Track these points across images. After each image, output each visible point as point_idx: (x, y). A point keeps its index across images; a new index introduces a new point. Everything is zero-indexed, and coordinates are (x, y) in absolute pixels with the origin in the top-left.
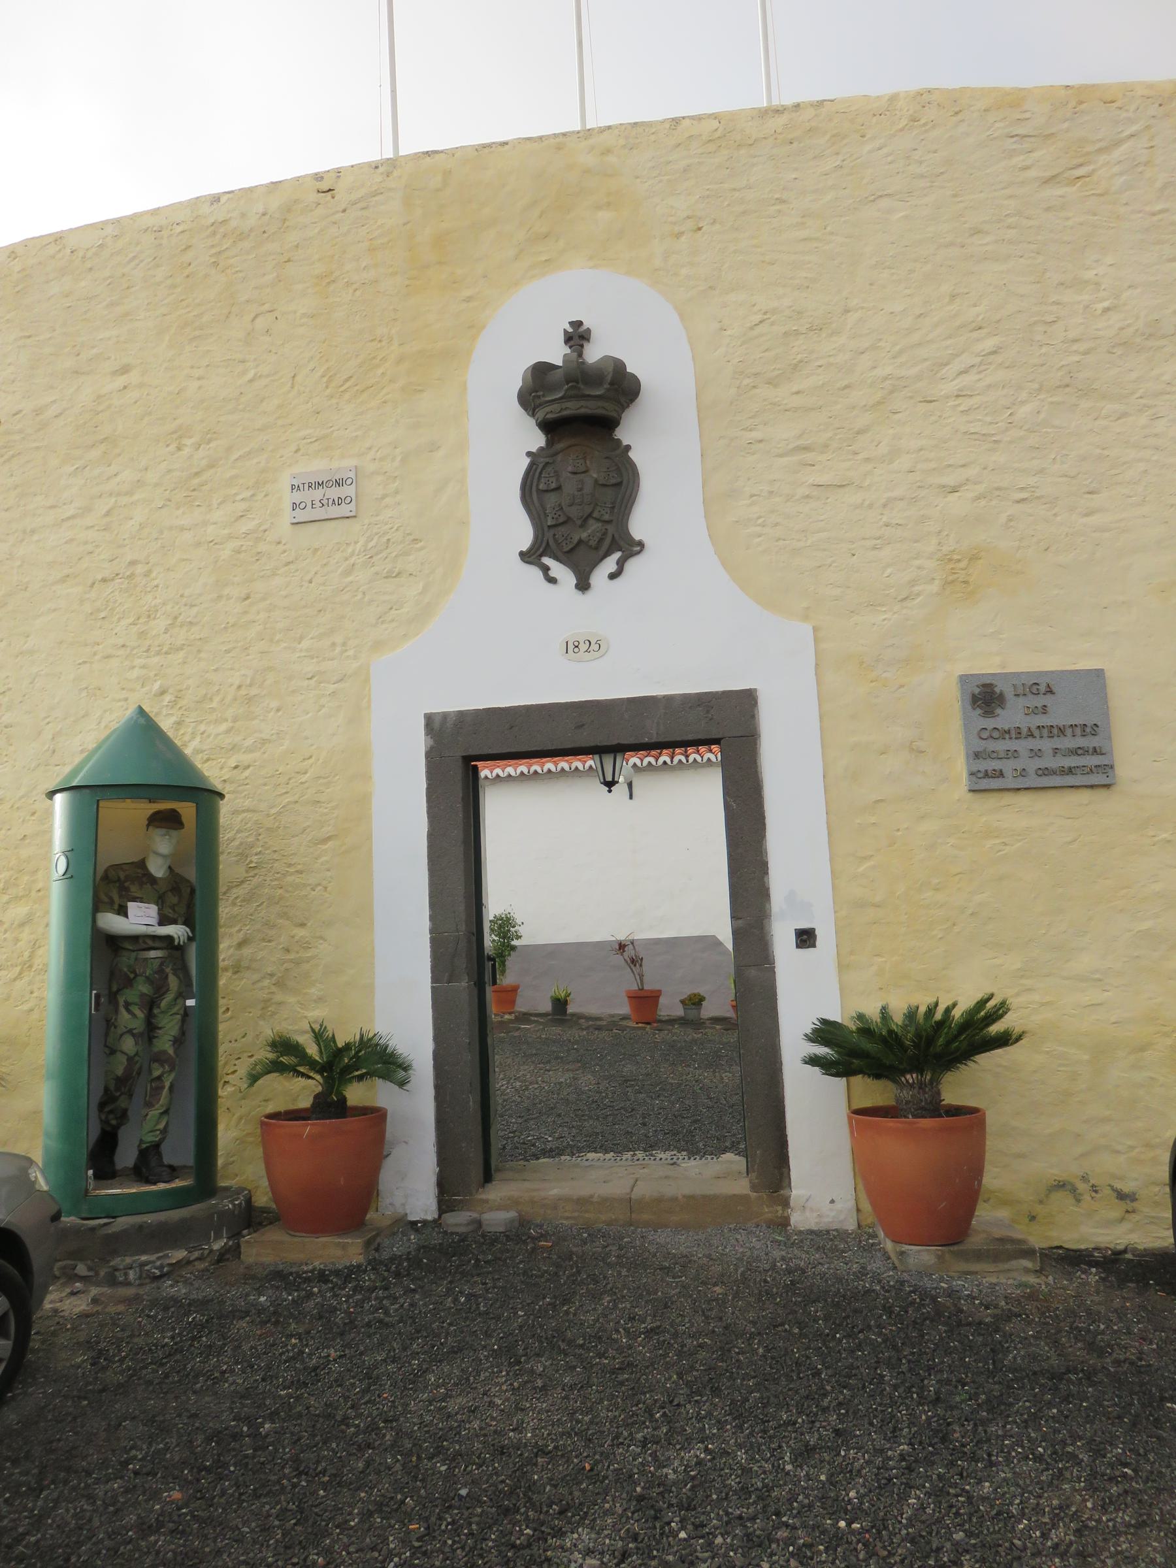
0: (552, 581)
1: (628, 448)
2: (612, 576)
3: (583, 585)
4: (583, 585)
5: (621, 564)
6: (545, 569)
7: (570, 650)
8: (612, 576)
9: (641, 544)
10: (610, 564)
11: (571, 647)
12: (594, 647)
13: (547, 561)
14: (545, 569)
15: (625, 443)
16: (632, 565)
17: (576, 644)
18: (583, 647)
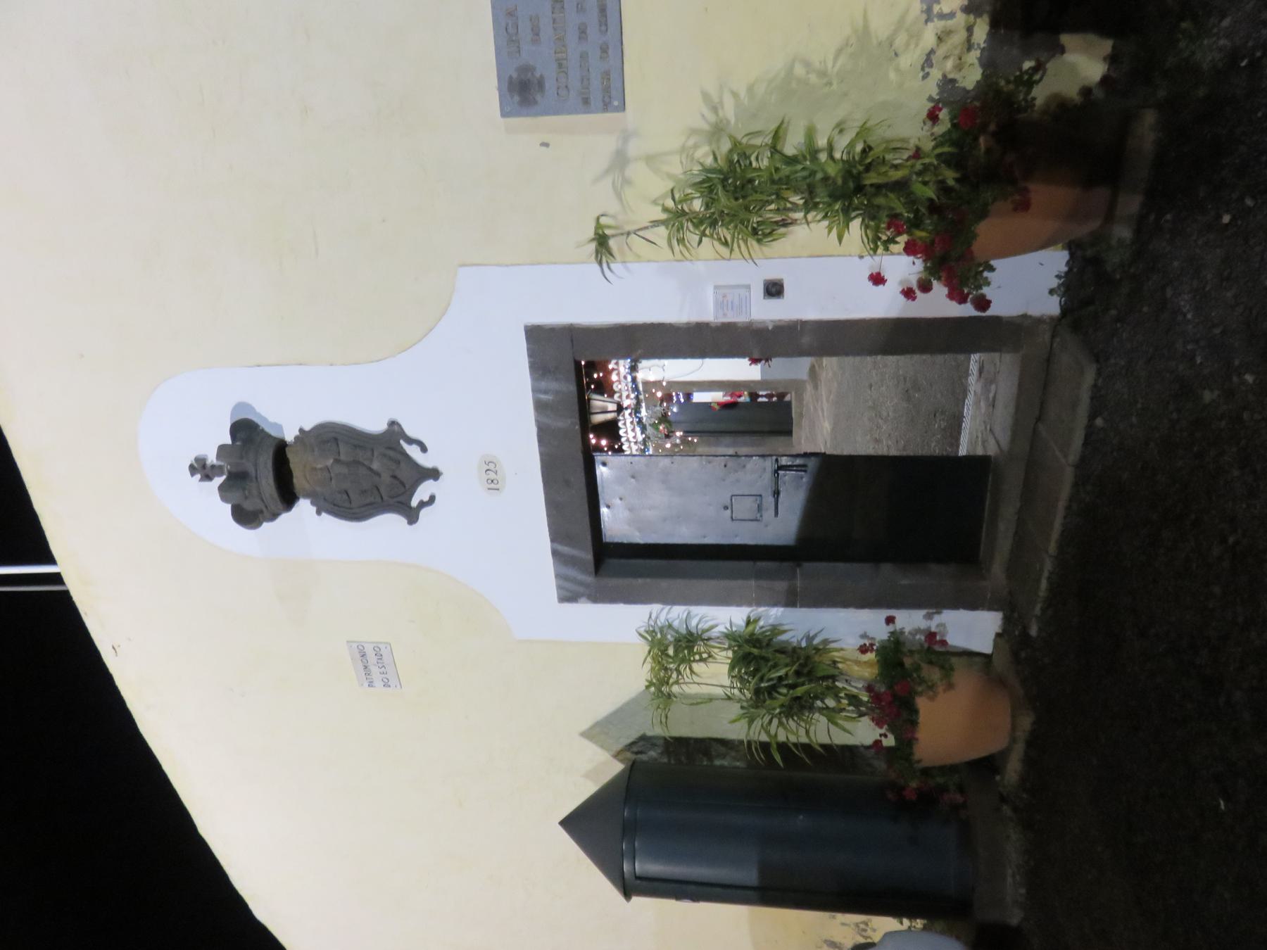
0: (432, 499)
1: (301, 430)
2: (424, 449)
3: (434, 474)
4: (434, 474)
5: (411, 441)
6: (422, 504)
7: (495, 486)
8: (424, 449)
9: (393, 423)
10: (413, 451)
11: (492, 486)
12: (491, 466)
13: (414, 503)
14: (422, 504)
15: (298, 433)
16: (410, 431)
17: (490, 481)
18: (492, 476)
